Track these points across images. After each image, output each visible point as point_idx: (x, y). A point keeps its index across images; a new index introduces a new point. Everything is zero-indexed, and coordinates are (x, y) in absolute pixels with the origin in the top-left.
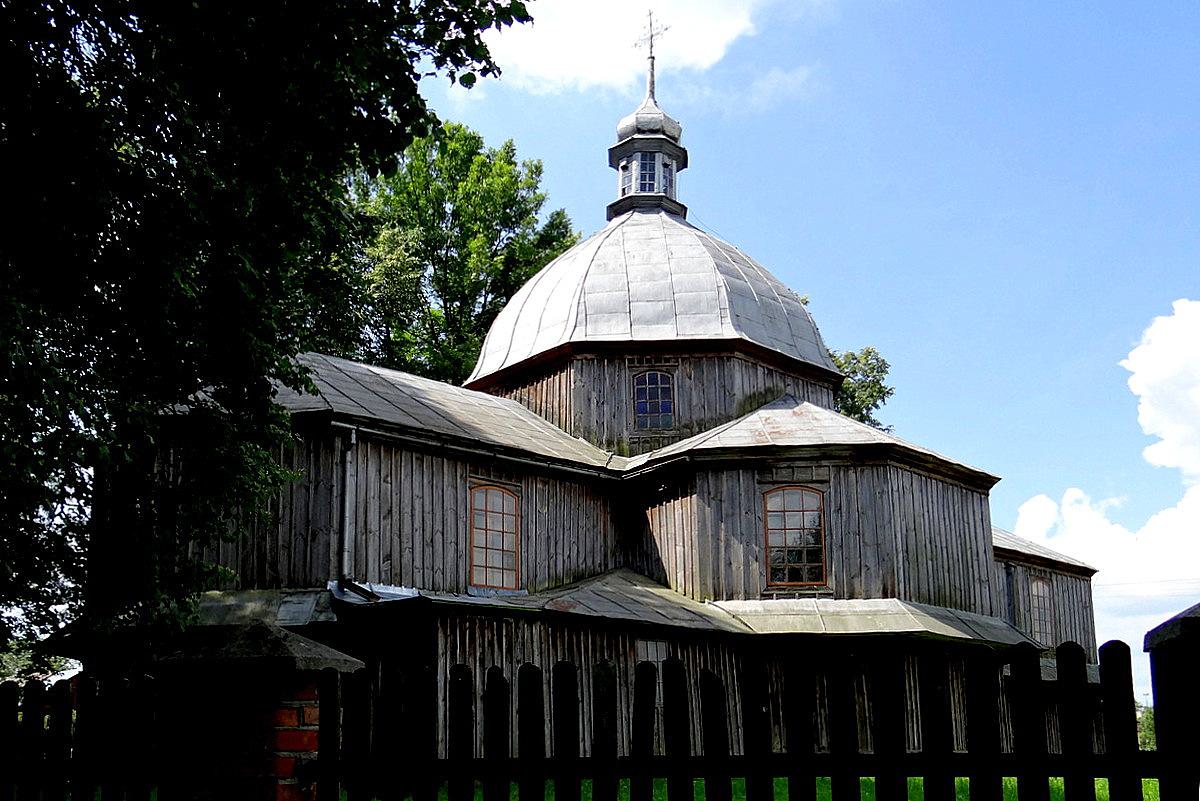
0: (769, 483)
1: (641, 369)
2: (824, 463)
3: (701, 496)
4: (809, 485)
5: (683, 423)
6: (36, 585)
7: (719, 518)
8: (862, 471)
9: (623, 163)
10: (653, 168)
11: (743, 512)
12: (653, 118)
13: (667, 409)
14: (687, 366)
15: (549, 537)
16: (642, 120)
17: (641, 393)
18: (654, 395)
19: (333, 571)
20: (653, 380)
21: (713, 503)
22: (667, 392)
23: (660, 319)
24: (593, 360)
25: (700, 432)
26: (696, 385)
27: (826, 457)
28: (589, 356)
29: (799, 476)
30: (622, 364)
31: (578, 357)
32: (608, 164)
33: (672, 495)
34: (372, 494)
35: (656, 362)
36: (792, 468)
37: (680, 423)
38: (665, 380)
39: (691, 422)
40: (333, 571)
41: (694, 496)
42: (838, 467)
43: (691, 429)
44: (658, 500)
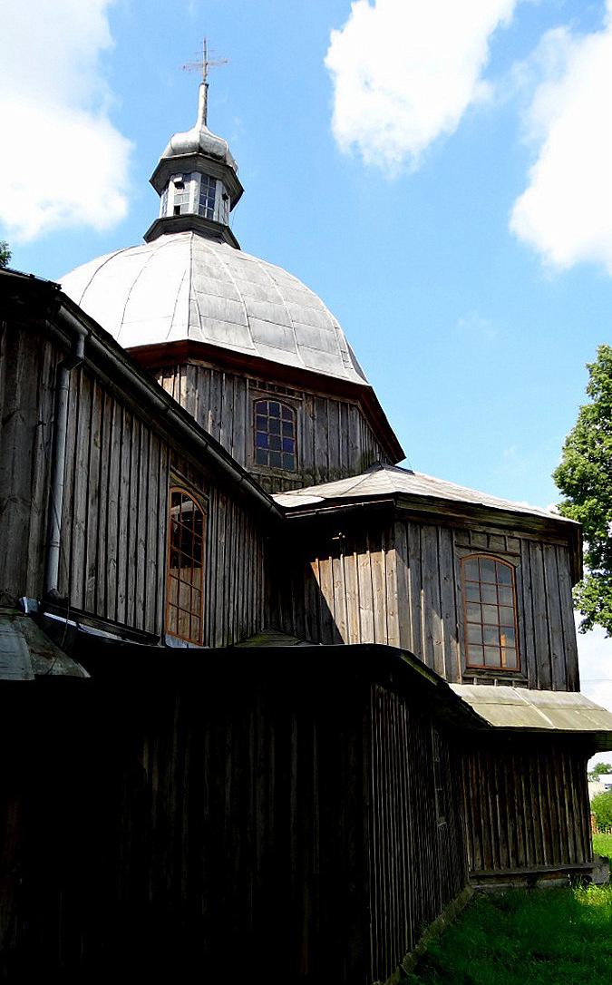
0: (466, 547)
1: (263, 395)
2: (516, 534)
3: (406, 558)
4: (502, 557)
5: (306, 468)
6: (62, 307)
7: (419, 585)
8: (547, 549)
9: (179, 179)
10: (212, 194)
11: (442, 579)
12: (216, 142)
13: (289, 446)
14: (310, 403)
15: (224, 577)
16: (205, 140)
17: (260, 422)
18: (275, 427)
19: (31, 583)
20: (274, 411)
21: (412, 562)
22: (289, 428)
23: (283, 344)
24: (210, 370)
25: (323, 482)
26: (319, 428)
27: (519, 528)
28: (205, 365)
29: (496, 545)
30: (242, 387)
31: (194, 363)
32: (150, 178)
33: (355, 545)
34: (80, 459)
35: (278, 391)
36: (487, 534)
37: (303, 466)
38: (287, 414)
39: (315, 468)
40: (31, 583)
41: (392, 552)
42: (528, 541)
43: (314, 476)
44: (334, 552)
